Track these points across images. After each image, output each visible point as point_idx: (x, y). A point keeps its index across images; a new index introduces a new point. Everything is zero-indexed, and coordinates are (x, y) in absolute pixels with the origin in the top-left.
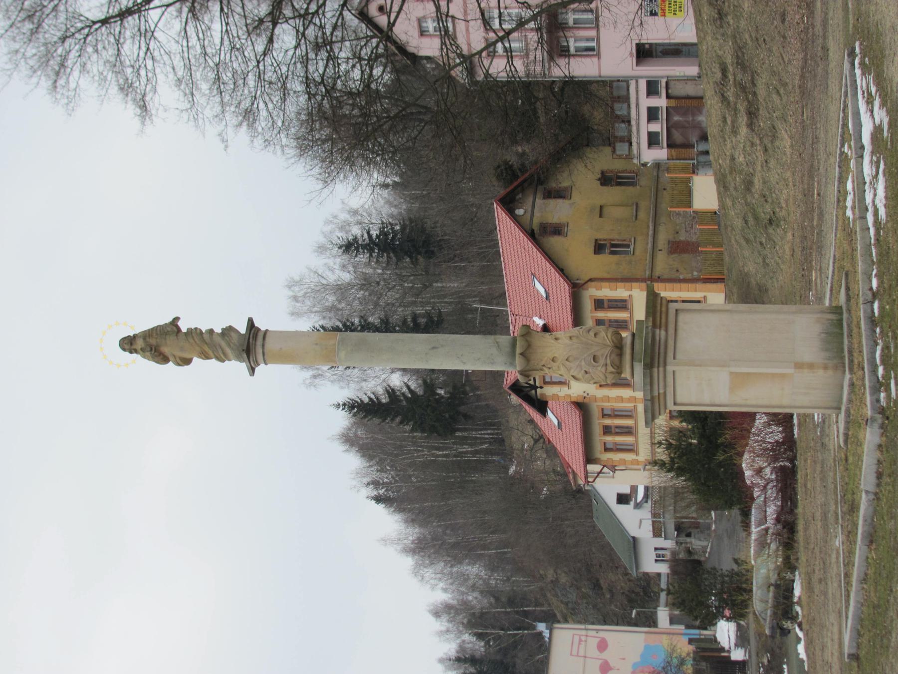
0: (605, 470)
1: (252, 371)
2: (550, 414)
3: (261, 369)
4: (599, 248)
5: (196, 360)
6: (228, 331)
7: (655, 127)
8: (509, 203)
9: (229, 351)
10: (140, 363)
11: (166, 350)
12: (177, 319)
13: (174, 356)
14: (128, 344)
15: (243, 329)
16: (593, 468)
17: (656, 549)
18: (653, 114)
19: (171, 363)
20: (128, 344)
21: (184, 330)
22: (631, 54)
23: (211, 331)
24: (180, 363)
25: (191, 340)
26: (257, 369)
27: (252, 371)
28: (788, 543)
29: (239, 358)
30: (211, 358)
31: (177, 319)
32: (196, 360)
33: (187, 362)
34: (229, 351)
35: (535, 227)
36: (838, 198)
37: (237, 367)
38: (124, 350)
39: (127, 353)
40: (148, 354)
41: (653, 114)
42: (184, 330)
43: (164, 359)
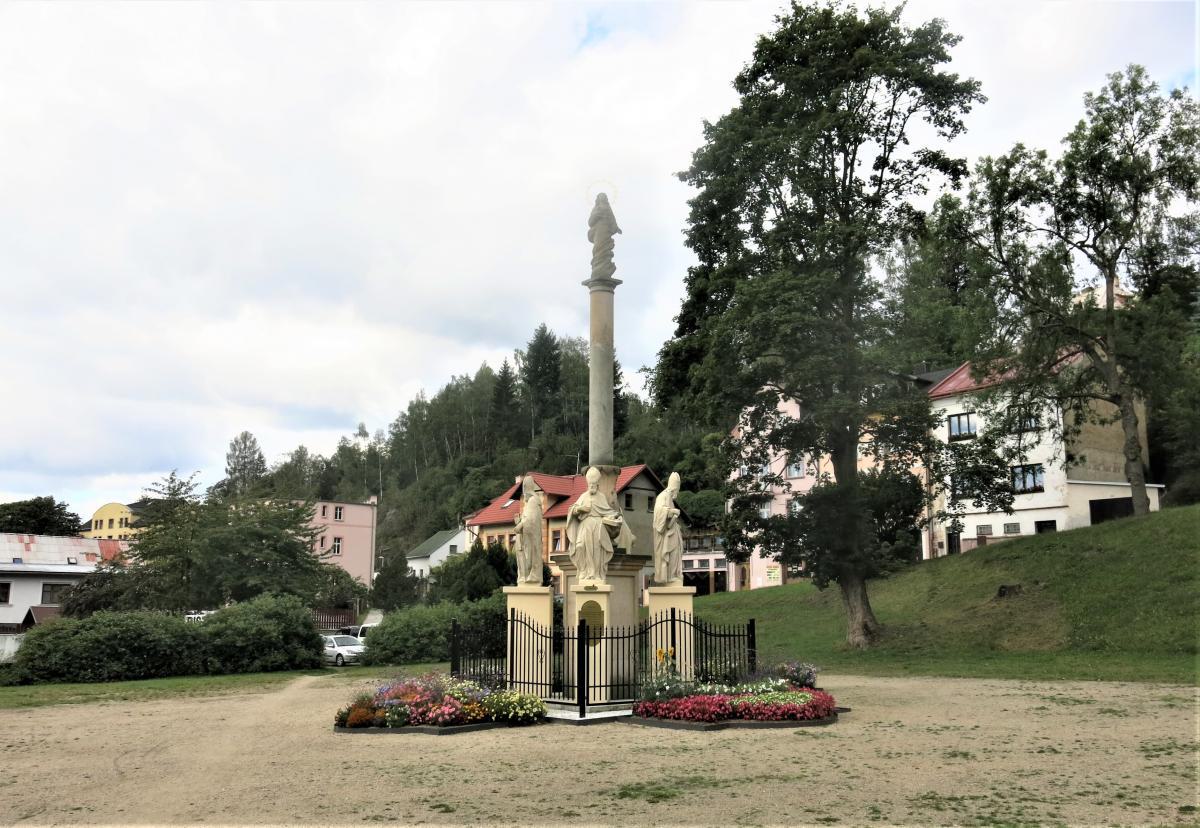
0: (475, 537)
2: (511, 502)
3: (587, 290)
4: (338, 540)
6: (613, 268)
7: (696, 565)
8: (645, 473)
9: (599, 267)
10: (588, 209)
12: (620, 232)
14: (602, 201)
16: (476, 529)
17: (101, 521)
18: (704, 563)
20: (602, 201)
21: (612, 237)
23: (612, 255)
27: (585, 283)
29: (593, 274)
31: (620, 232)
33: (591, 239)
34: (599, 267)
35: (631, 491)
36: (977, 798)
37: (588, 275)
40: (596, 212)
41: (704, 563)
42: (612, 237)
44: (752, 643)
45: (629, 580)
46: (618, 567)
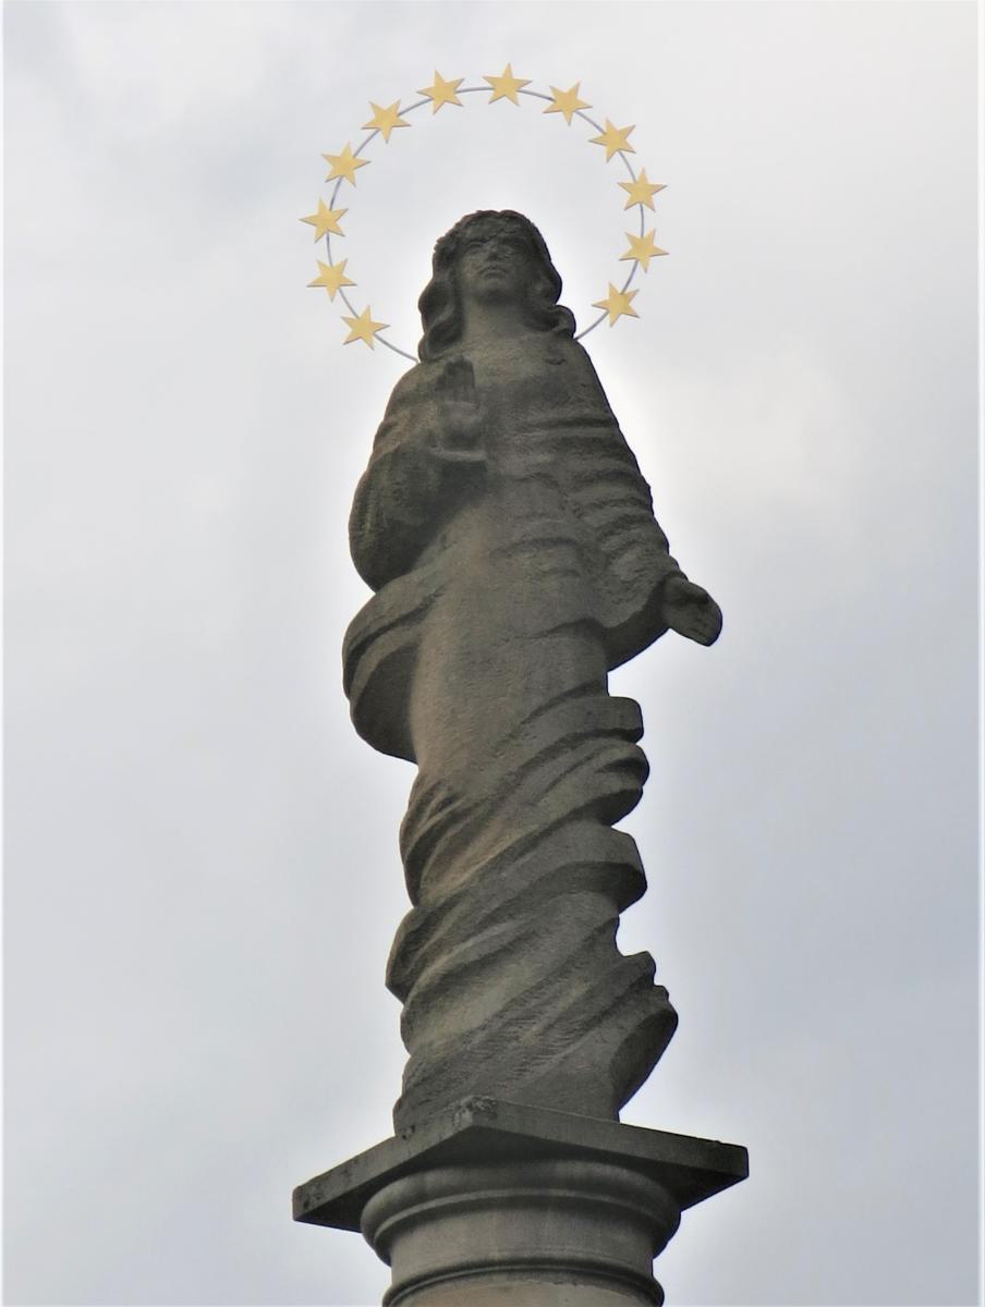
1: (330, 1203)
5: (400, 776)
11: (463, 548)
12: (699, 617)
13: (416, 615)
14: (496, 275)
15: (655, 1107)
19: (366, 593)
20: (496, 275)
21: (622, 681)
22: (545, 824)
24: (371, 661)
25: (547, 732)
26: (353, 1244)
27: (330, 1203)
28: (555, 323)
30: (360, 1232)
31: (699, 617)
32: (400, 776)
33: (381, 720)
38: (449, 253)
39: (423, 274)
42: (622, 681)
43: (387, 537)
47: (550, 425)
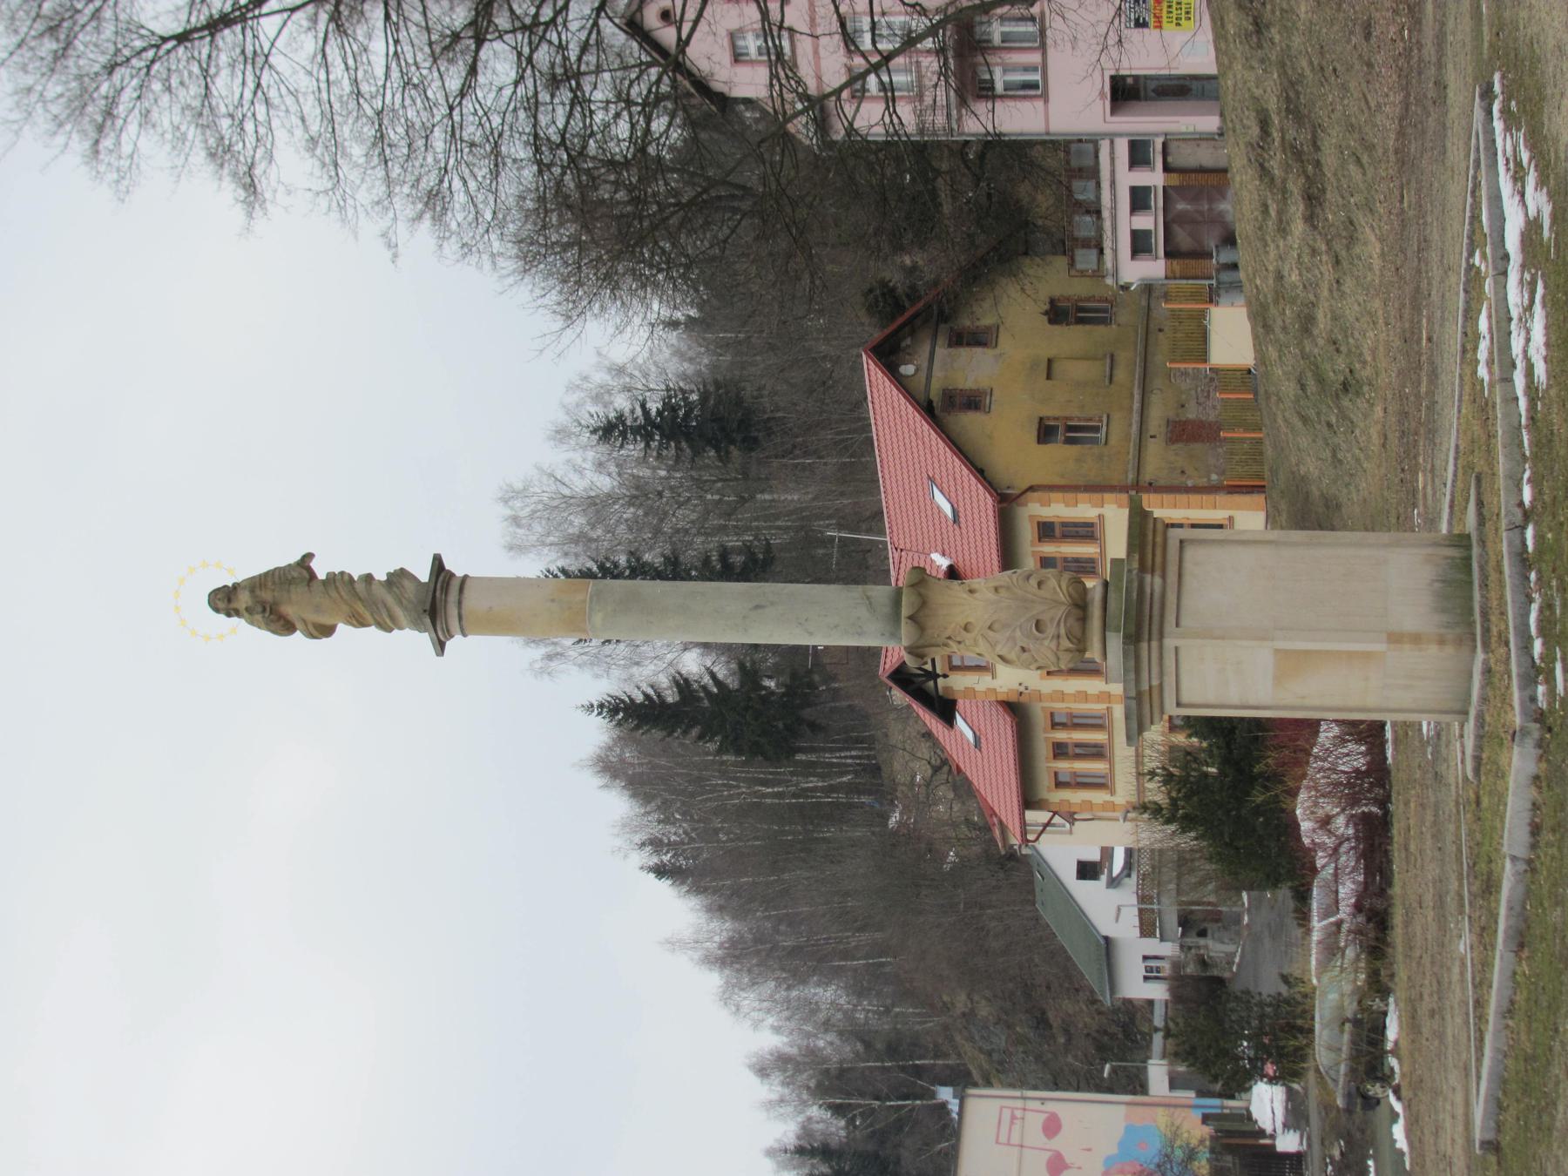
1: (440, 647)
2: (960, 722)
3: (455, 644)
4: (1046, 433)
5: (342, 628)
6: (399, 578)
7: (1144, 222)
8: (889, 355)
9: (399, 613)
10: (244, 634)
11: (289, 611)
12: (309, 556)
13: (304, 621)
14: (224, 600)
15: (424, 575)
17: (1145, 958)
18: (1139, 199)
19: (298, 633)
20: (224, 600)
21: (321, 576)
23: (369, 578)
24: (315, 633)
25: (334, 594)
26: (448, 644)
27: (440, 647)
28: (1375, 948)
29: (417, 625)
30: (369, 625)
31: (309, 556)
32: (342, 628)
33: (326, 631)
34: (399, 613)
35: (935, 395)
36: (1463, 346)
37: (413, 641)
38: (217, 610)
39: (222, 616)
40: (259, 617)
41: (1139, 199)
42: (321, 576)
43: (287, 627)
44: (1176, 1106)
45: (1190, 553)
46: (1158, 580)
47: (1150, 640)
